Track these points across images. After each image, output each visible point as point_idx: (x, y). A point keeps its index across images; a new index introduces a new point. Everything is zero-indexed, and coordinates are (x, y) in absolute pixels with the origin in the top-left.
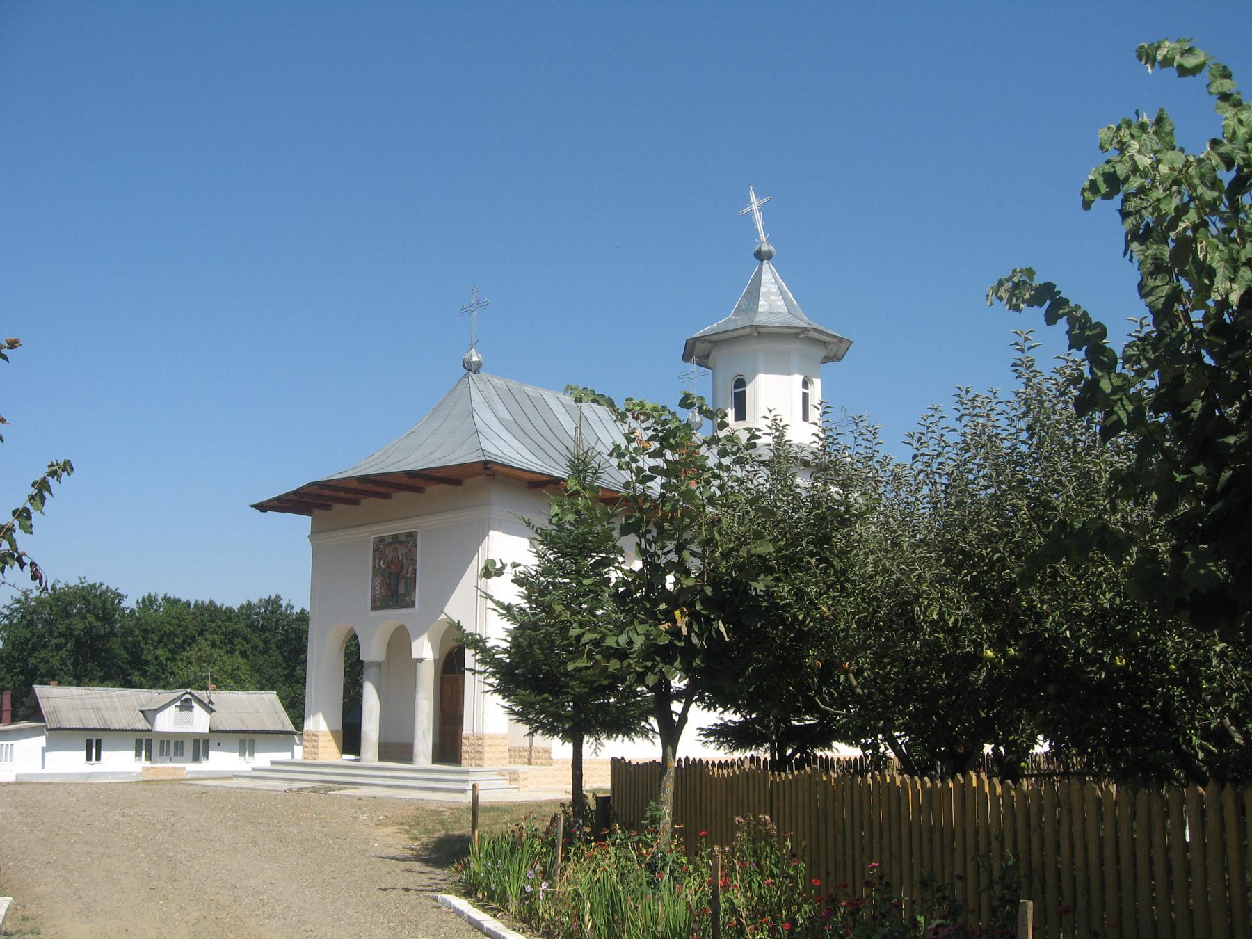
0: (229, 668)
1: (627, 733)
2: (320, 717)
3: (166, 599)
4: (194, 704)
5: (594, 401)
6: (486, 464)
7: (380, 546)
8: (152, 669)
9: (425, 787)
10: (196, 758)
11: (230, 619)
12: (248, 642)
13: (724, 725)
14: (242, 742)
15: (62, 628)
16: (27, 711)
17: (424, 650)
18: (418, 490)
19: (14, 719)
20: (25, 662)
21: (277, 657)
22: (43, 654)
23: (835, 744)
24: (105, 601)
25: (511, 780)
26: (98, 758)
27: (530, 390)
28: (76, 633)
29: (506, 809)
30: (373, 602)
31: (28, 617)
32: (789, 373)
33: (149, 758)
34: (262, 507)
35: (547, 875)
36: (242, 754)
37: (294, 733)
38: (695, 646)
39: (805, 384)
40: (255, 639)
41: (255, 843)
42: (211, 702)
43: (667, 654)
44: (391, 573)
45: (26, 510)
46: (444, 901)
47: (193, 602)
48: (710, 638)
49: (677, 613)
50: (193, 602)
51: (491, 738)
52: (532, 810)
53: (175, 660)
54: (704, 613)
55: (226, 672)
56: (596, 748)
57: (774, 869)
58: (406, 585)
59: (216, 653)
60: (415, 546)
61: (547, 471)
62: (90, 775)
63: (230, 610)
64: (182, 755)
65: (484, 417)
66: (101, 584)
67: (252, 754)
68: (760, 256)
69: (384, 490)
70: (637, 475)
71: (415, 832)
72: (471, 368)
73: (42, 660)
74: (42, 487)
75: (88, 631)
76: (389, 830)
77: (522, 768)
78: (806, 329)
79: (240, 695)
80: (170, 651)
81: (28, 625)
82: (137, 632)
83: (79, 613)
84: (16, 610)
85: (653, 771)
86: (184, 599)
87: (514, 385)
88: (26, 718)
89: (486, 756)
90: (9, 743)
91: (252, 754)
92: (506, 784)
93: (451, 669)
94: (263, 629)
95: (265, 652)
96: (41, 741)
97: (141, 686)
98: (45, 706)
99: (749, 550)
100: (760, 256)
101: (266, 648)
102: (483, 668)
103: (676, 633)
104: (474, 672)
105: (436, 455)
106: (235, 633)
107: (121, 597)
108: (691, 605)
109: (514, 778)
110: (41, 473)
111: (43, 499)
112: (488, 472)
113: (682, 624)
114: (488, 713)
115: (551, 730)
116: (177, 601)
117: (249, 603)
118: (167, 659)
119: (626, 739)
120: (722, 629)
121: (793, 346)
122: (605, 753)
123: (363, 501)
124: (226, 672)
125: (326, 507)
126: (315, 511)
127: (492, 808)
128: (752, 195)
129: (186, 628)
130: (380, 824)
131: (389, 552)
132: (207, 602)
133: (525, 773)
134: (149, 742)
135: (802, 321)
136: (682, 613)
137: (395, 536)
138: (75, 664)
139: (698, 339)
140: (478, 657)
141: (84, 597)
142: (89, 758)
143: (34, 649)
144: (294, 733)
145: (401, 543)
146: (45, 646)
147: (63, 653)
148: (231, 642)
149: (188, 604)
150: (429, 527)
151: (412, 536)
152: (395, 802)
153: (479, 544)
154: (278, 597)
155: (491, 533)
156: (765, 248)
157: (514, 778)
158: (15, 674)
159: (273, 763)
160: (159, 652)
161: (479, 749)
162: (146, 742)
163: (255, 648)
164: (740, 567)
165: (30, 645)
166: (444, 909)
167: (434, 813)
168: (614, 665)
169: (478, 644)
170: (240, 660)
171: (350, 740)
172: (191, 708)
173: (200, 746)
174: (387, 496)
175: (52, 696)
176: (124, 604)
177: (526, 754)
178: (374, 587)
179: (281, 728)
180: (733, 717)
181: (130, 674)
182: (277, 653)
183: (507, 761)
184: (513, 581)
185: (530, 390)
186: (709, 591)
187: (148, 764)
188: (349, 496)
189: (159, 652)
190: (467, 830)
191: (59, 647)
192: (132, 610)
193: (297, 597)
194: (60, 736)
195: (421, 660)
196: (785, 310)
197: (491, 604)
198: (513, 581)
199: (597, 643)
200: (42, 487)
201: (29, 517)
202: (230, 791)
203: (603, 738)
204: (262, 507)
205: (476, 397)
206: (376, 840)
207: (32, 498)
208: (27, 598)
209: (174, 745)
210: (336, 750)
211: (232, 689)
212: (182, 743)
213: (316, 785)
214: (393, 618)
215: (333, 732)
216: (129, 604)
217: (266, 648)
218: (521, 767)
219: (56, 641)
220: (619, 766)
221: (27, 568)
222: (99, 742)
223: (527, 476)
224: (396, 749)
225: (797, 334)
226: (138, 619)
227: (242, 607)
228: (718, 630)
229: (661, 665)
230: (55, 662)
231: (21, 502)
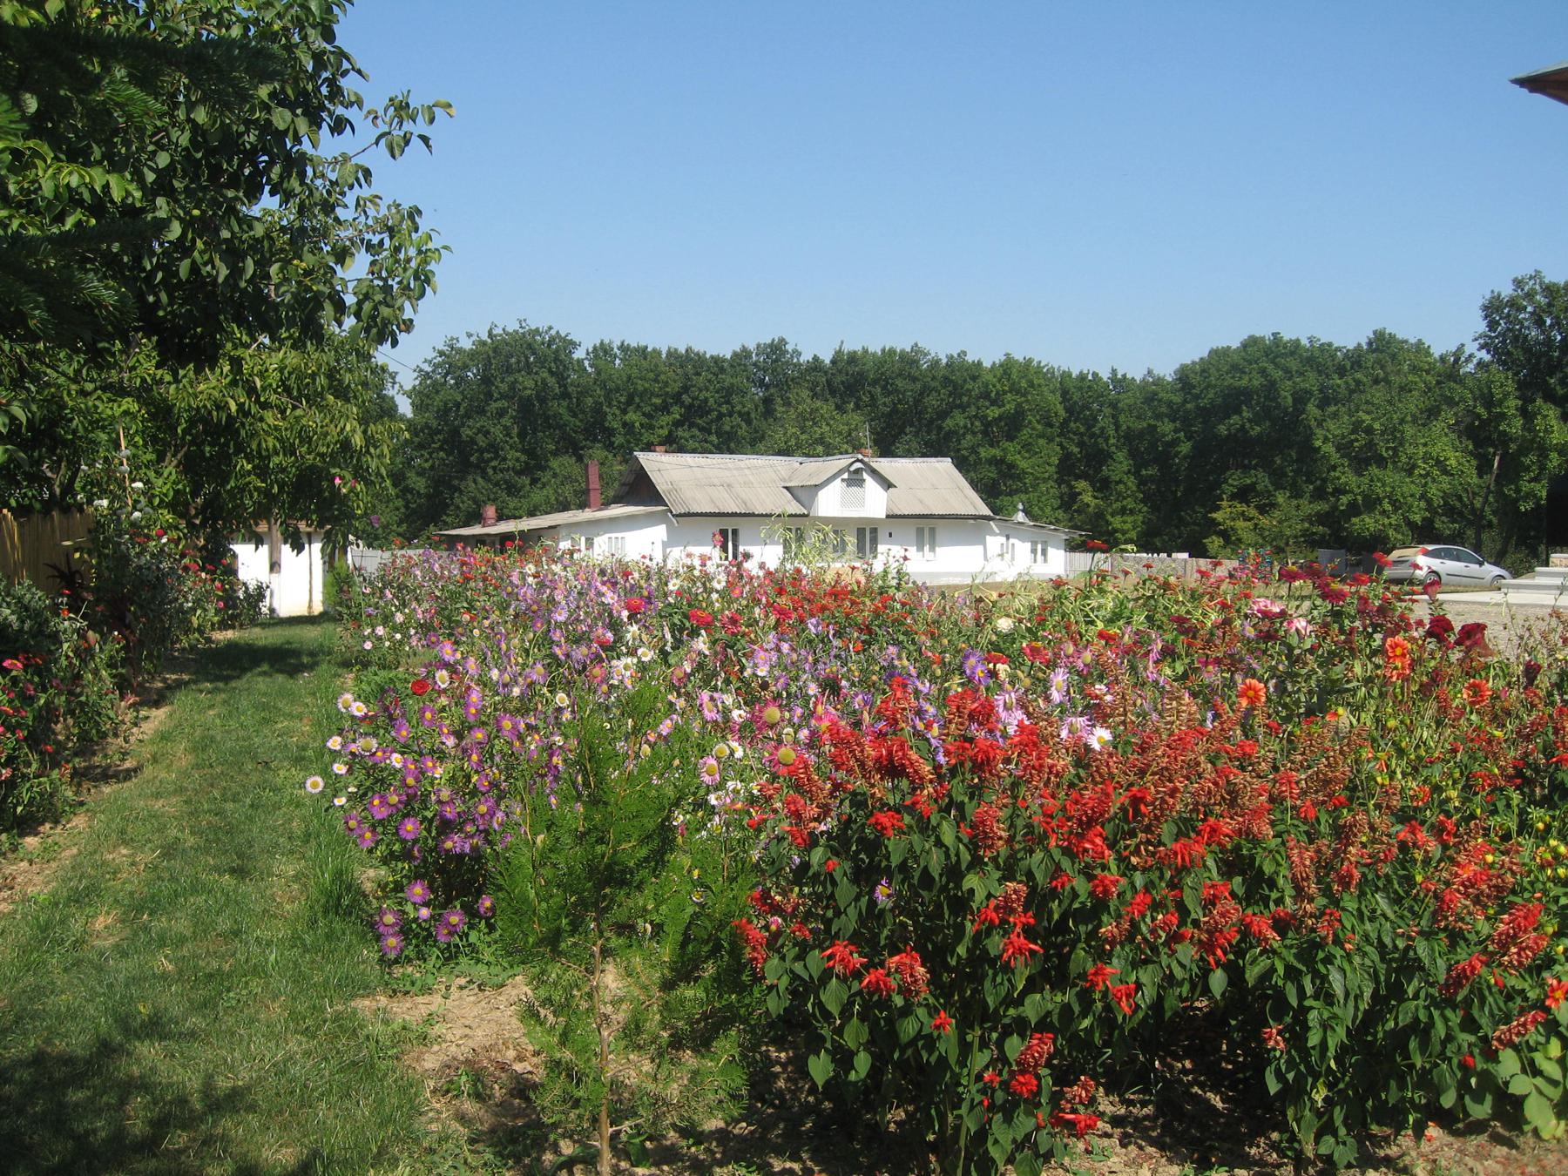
3: (623, 347)
4: (865, 476)
11: (722, 370)
14: (920, 531)
15: (504, 387)
16: (640, 490)
22: (481, 422)
34: (1535, 84)
67: (932, 549)
73: (479, 431)
80: (644, 414)
88: (619, 500)
90: (620, 535)
91: (932, 549)
98: (660, 482)
116: (642, 352)
117: (744, 349)
124: (840, 433)
138: (522, 435)
154: (783, 341)
179: (972, 512)
191: (501, 413)
204: (1535, 84)
212: (874, 531)
219: (499, 404)
222: (735, 532)
227: (735, 354)
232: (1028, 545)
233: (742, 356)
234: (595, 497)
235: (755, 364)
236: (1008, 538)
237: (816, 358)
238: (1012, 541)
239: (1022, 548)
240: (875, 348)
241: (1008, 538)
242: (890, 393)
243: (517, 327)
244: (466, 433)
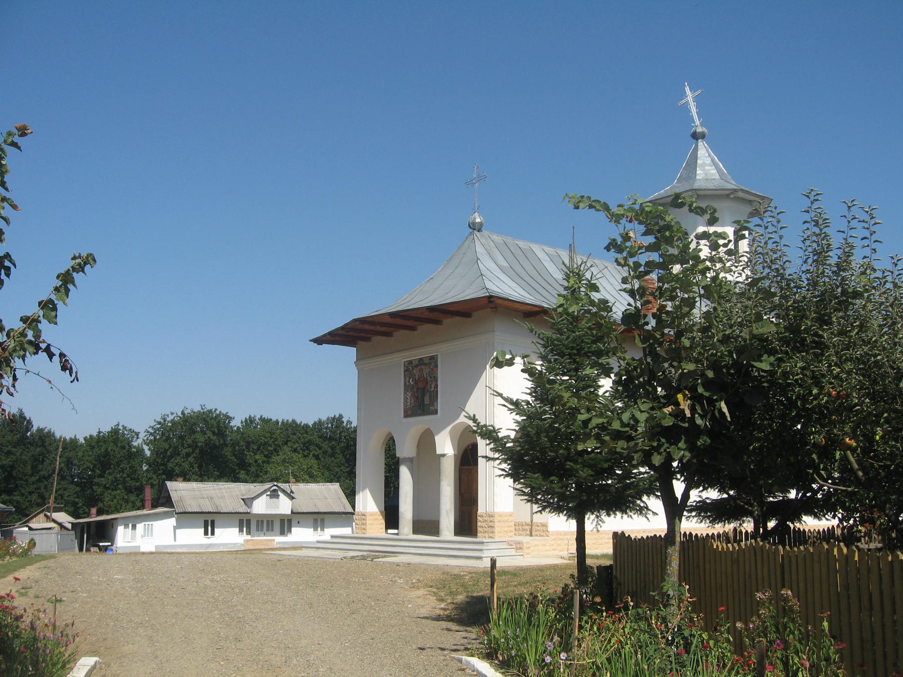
0: (305, 467)
1: (624, 512)
3: (261, 419)
4: (280, 493)
5: (591, 207)
6: (490, 297)
7: (409, 368)
8: (253, 469)
9: (447, 554)
10: (282, 533)
11: (306, 432)
12: (320, 448)
13: (703, 502)
14: (315, 520)
15: (190, 441)
16: (163, 500)
17: (446, 446)
18: (437, 322)
19: (154, 506)
20: (165, 465)
21: (341, 458)
22: (178, 460)
23: (805, 518)
24: (219, 422)
26: (213, 533)
27: (521, 244)
28: (200, 444)
29: (515, 573)
30: (405, 411)
31: (167, 434)
33: (249, 533)
34: (319, 341)
35: (566, 646)
36: (315, 529)
38: (699, 426)
40: (325, 446)
41: (311, 605)
42: (292, 492)
43: (671, 434)
44: (418, 388)
45: (51, 301)
46: (468, 663)
47: (280, 421)
48: (713, 419)
49: (680, 397)
50: (280, 421)
51: (500, 516)
52: (540, 573)
53: (268, 463)
54: (707, 394)
56: (598, 524)
57: (798, 645)
58: (430, 397)
59: (295, 456)
60: (437, 366)
61: (538, 303)
62: (210, 545)
63: (307, 426)
64: (272, 530)
65: (486, 264)
66: (216, 410)
67: (322, 530)
68: (696, 136)
69: (409, 323)
70: (635, 270)
71: (442, 594)
72: (475, 228)
73: (177, 464)
74: (66, 279)
75: (208, 442)
76: (421, 592)
77: (525, 539)
78: (735, 190)
79: (312, 486)
80: (265, 456)
81: (167, 440)
82: (242, 443)
83: (202, 431)
84: (158, 429)
85: (654, 547)
86: (274, 419)
87: (509, 240)
88: (163, 505)
89: (497, 530)
91: (322, 530)
92: (513, 552)
93: (467, 460)
94: (331, 439)
95: (333, 455)
96: (172, 521)
97: (246, 481)
98: (174, 496)
99: (751, 332)
100: (696, 136)
101: (328, 452)
102: (497, 455)
103: (678, 414)
104: (488, 459)
105: (449, 295)
106: (310, 442)
107: (231, 419)
108: (693, 389)
109: (519, 547)
110: (67, 264)
111: (67, 291)
112: (491, 305)
113: (685, 405)
114: (499, 492)
115: (558, 509)
117: (320, 421)
118: (263, 462)
119: (625, 516)
120: (725, 409)
122: (604, 530)
123: (395, 333)
125: (368, 339)
126: (359, 342)
127: (504, 572)
128: (687, 89)
129: (276, 440)
130: (414, 587)
131: (416, 372)
132: (290, 420)
133: (528, 543)
134: (249, 521)
135: (732, 185)
136: (685, 396)
138: (200, 467)
140: (492, 446)
141: (204, 420)
142: (206, 533)
143: (171, 456)
145: (426, 364)
146: (179, 455)
147: (191, 459)
148: (308, 449)
149: (277, 422)
150: (446, 352)
151: (433, 359)
152: (426, 568)
154: (341, 416)
156: (699, 130)
157: (519, 547)
158: (159, 474)
159: (332, 537)
160: (257, 457)
161: (490, 524)
162: (246, 522)
164: (740, 351)
165: (169, 453)
166: (467, 671)
167: (457, 577)
168: (621, 444)
169: (490, 434)
170: (314, 462)
171: (391, 518)
172: (277, 496)
173: (285, 524)
174: (413, 329)
175: (178, 489)
176: (232, 424)
177: (528, 528)
179: (343, 510)
180: (713, 494)
181: (238, 473)
182: (341, 456)
183: (513, 534)
184: (523, 371)
185: (521, 244)
186: (710, 374)
187: (249, 537)
188: (383, 329)
189: (257, 457)
190: (486, 592)
191: (188, 455)
192: (238, 428)
193: (351, 415)
194: (186, 518)
195: (444, 455)
196: (717, 177)
197: (500, 400)
198: (523, 371)
199: (602, 427)
200: (66, 279)
201: (55, 309)
202: (299, 559)
203: (603, 514)
204: (319, 341)
205: (480, 249)
206: (409, 602)
207: (57, 289)
208: (165, 420)
209: (267, 523)
211: (308, 482)
212: (272, 521)
213: (365, 553)
214: (420, 423)
216: (236, 423)
217: (328, 452)
218: (531, 538)
219: (187, 450)
220: (619, 539)
221: (56, 359)
222: (213, 522)
223: (523, 308)
224: (426, 525)
225: (728, 196)
226: (243, 434)
227: (315, 423)
228: (720, 410)
229: (666, 445)
230: (186, 466)
231: (46, 293)
233: (319, 424)
234: (148, 504)
243: (200, 409)
244: (170, 465)
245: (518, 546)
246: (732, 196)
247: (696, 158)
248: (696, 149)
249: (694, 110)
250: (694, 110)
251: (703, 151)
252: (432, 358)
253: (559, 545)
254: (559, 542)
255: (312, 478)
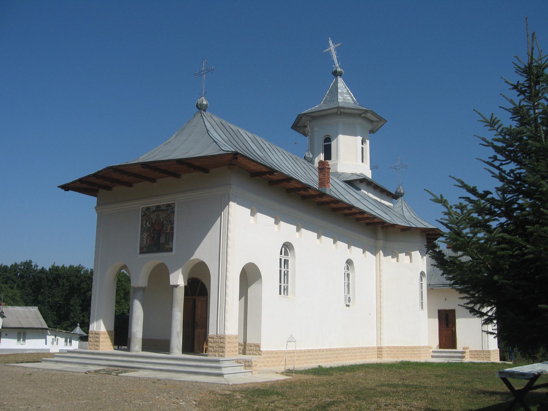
0: (10, 295)
2: (101, 323)
7: (146, 213)
11: (6, 271)
14: (19, 334)
17: (179, 279)
18: (176, 175)
25: (245, 366)
32: (356, 135)
34: (66, 187)
36: (19, 340)
37: (47, 329)
39: (363, 142)
51: (229, 338)
55: (9, 297)
60: (173, 212)
63: (6, 267)
68: (336, 74)
78: (366, 111)
87: (224, 122)
89: (227, 350)
91: (24, 340)
92: (242, 369)
95: (23, 288)
100: (336, 74)
117: (16, 264)
121: (359, 121)
124: (9, 297)
125: (108, 188)
126: (101, 191)
137: (158, 207)
139: (305, 114)
144: (47, 329)
145: (162, 211)
150: (183, 201)
153: (222, 209)
154: (31, 261)
155: (231, 203)
156: (339, 70)
161: (221, 345)
163: (18, 286)
171: (121, 336)
178: (142, 240)
179: (40, 326)
182: (29, 289)
183: (238, 353)
185: (231, 126)
195: (176, 286)
204: (66, 187)
210: (111, 344)
214: (155, 258)
215: (109, 332)
224: (157, 344)
227: (12, 266)
232: (64, 339)
233: (15, 266)
235: (20, 269)
236: (56, 337)
237: (43, 268)
238: (57, 337)
239: (62, 340)
240: (67, 265)
241: (56, 337)
242: (69, 282)
245: (247, 364)
246: (363, 115)
247: (337, 88)
248: (336, 83)
249: (335, 57)
250: (335, 57)
251: (341, 83)
252: (169, 205)
253: (268, 362)
254: (268, 360)
255: (14, 302)
